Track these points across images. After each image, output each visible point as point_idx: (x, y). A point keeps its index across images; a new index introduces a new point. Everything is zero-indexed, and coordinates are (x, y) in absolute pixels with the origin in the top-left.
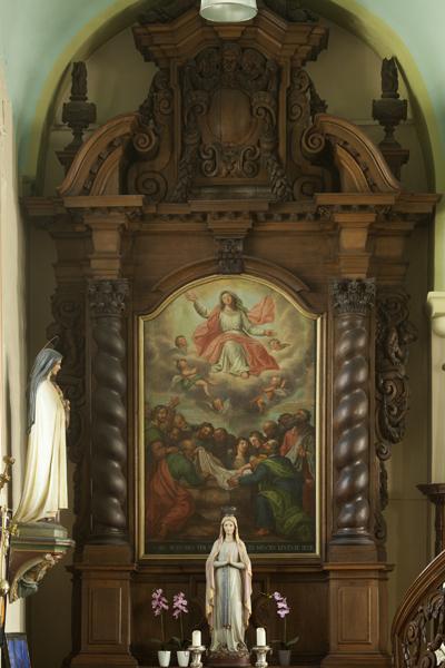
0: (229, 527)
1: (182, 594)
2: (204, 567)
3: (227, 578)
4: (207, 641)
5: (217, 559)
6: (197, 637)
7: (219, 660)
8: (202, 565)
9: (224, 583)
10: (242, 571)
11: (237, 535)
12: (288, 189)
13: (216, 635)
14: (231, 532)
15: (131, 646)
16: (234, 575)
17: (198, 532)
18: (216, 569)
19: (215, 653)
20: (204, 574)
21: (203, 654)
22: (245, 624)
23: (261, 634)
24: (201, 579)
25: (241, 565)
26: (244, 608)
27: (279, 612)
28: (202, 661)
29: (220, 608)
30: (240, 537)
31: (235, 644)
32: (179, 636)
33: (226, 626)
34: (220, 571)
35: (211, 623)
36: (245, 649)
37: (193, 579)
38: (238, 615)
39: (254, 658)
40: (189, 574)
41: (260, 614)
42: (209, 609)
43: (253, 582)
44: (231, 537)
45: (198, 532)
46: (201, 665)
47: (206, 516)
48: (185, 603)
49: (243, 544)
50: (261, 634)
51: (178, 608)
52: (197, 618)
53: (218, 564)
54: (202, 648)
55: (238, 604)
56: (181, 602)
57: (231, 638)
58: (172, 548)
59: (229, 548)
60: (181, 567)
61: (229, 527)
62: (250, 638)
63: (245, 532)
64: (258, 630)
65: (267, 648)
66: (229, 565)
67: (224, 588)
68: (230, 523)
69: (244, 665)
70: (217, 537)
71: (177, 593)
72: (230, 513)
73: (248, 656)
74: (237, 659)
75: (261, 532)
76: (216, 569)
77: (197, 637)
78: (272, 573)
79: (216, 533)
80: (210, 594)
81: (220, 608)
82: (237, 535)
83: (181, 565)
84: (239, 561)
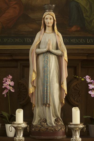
0: (49, 20)
1: (11, 77)
2: (28, 55)
3: (47, 63)
4: (29, 117)
5: (38, 47)
6: (20, 114)
7: (39, 133)
8: (27, 53)
9: (44, 68)
10: (59, 57)
11: (56, 27)
12: (44, 69)
13: (37, 111)
14: (51, 25)
15: (50, 106)
16: (53, 60)
17: (25, 28)
18: (38, 55)
19: (36, 126)
20: (28, 60)
21: (25, 129)
22: (61, 102)
23: (76, 113)
24: (26, 65)
25: (59, 52)
26: (61, 88)
27: (90, 92)
28: (24, 136)
29: (41, 88)
30: (59, 30)
31: (53, 119)
32: (7, 112)
33: (46, 104)
34: (41, 57)
35: (33, 101)
36: (61, 123)
37: (19, 64)
38: (56, 95)
39: (69, 134)
40: (17, 60)
41: (75, 94)
42: (31, 90)
43: (68, 67)
44: (51, 29)
45: (25, 28)
46: (23, 139)
47: (32, 16)
48: (12, 83)
49: (60, 35)
50: (76, 113)
51: (6, 88)
52: (22, 98)
53: (39, 51)
54: (24, 125)
55: (56, 86)
56: (9, 83)
57: (49, 114)
58: (5, 40)
59: (49, 39)
60: (11, 55)
61: (49, 20)
62: (67, 116)
63: (62, 26)
64: (74, 109)
65: (81, 126)
66: (49, 52)
67: (44, 72)
68: (50, 17)
69: (60, 137)
70: (39, 30)
71: (6, 76)
72: (50, 9)
73: (63, 130)
74: (55, 132)
75: (74, 29)
76: (38, 55)
77: (20, 114)
78: (83, 61)
79: (39, 25)
80: (33, 76)
81: (41, 88)
82: (56, 27)
83: (11, 53)
84: (57, 48)
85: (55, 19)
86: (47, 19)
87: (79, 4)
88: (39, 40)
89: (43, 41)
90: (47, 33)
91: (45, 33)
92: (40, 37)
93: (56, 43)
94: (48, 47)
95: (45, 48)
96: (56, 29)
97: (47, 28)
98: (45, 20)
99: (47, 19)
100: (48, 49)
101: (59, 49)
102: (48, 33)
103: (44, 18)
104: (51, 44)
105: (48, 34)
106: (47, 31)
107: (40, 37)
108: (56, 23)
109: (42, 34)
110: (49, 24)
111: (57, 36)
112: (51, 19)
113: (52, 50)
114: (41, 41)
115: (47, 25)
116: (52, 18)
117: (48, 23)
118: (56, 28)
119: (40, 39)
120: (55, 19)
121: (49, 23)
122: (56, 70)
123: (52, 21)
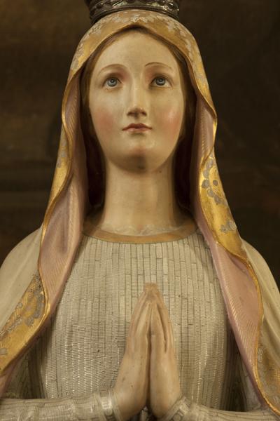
11: (208, 177)
14: (161, 145)
44: (155, 189)
68: (137, 79)
82: (208, 177)
85: (203, 85)
86: (115, 78)
87: (71, 156)
88: (36, 314)
89: (72, 314)
90: (117, 238)
91: (92, 244)
92: (38, 277)
93: (222, 345)
94: (132, 369)
95: (107, 387)
96: (218, 201)
97: (119, 185)
98: (102, 101)
99: (115, 78)
100: (141, 395)
101: (251, 396)
102: (128, 240)
103: (86, 71)
104: (174, 338)
105: (126, 248)
106: (116, 216)
107: (38, 277)
108: (210, 127)
109: (63, 247)
110: (138, 129)
111: (222, 263)
112: (157, 80)
113: (183, 407)
114: (60, 319)
115: (119, 143)
116: (173, 71)
117: (127, 121)
118: (218, 189)
119: (43, 300)
120: (203, 85)
121: (147, 122)
122: (217, 373)
123: (173, 101)
